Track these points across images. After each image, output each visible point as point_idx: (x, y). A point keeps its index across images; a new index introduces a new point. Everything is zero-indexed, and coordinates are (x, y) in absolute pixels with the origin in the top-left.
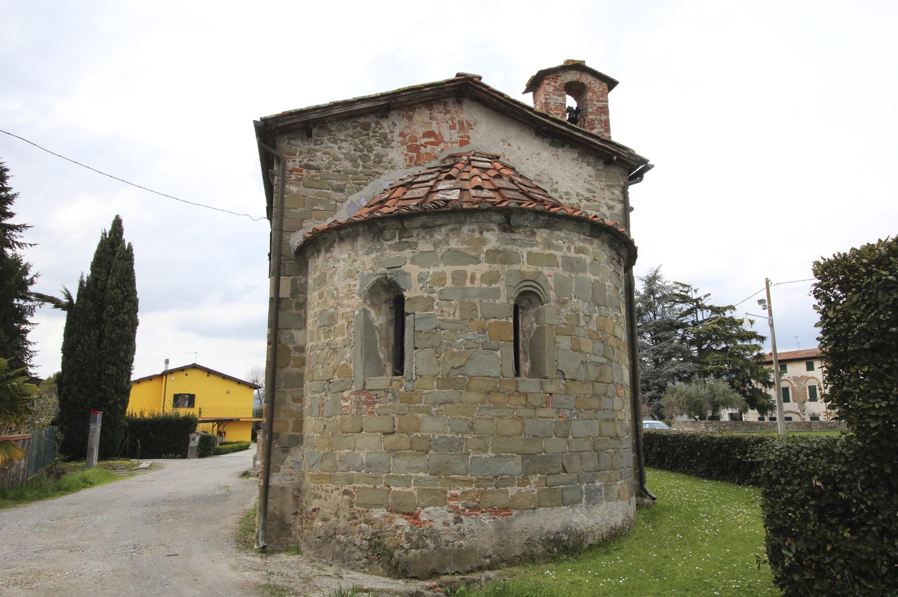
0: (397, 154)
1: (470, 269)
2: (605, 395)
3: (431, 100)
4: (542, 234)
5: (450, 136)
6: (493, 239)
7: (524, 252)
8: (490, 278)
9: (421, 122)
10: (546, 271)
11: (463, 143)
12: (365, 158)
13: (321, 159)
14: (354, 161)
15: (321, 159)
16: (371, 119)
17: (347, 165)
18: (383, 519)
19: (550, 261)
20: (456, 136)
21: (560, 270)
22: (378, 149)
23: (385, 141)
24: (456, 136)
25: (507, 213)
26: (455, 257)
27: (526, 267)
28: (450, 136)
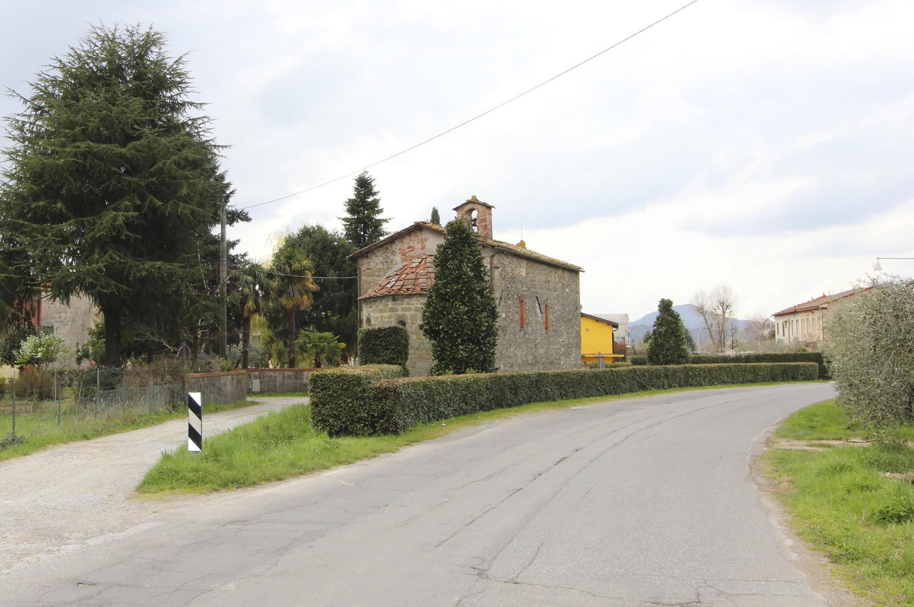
0: (398, 258)
1: (384, 314)
2: (525, 333)
3: (367, 253)
4: (406, 300)
5: (418, 246)
6: (390, 304)
7: (400, 307)
8: (390, 317)
9: (407, 242)
10: (407, 313)
11: (423, 248)
12: (387, 262)
13: (372, 265)
14: (383, 264)
15: (372, 265)
16: (388, 245)
17: (380, 266)
18: (773, 320)
19: (410, 309)
20: (420, 246)
21: (413, 312)
22: (391, 257)
23: (394, 253)
24: (420, 246)
25: (394, 295)
26: (381, 311)
27: (400, 313)
28: (418, 246)
